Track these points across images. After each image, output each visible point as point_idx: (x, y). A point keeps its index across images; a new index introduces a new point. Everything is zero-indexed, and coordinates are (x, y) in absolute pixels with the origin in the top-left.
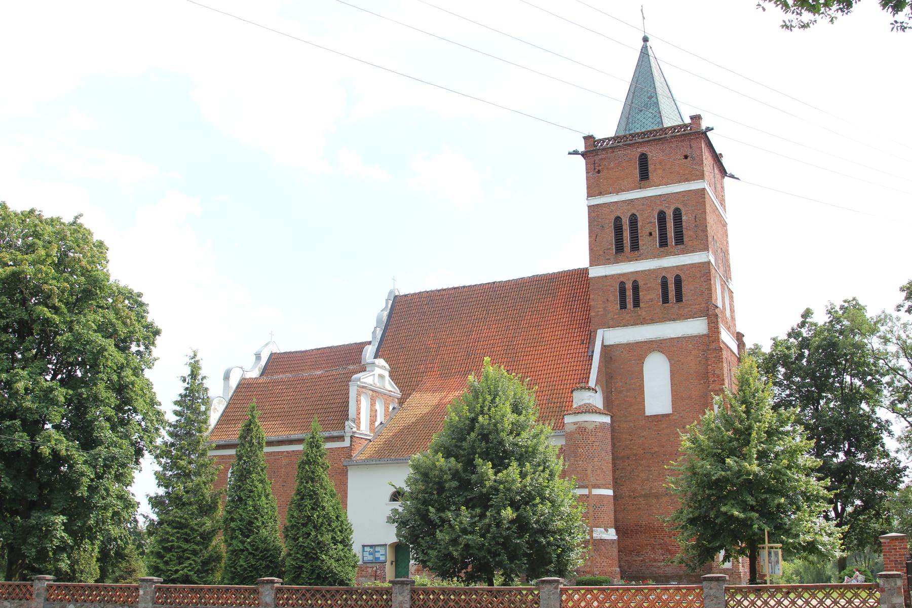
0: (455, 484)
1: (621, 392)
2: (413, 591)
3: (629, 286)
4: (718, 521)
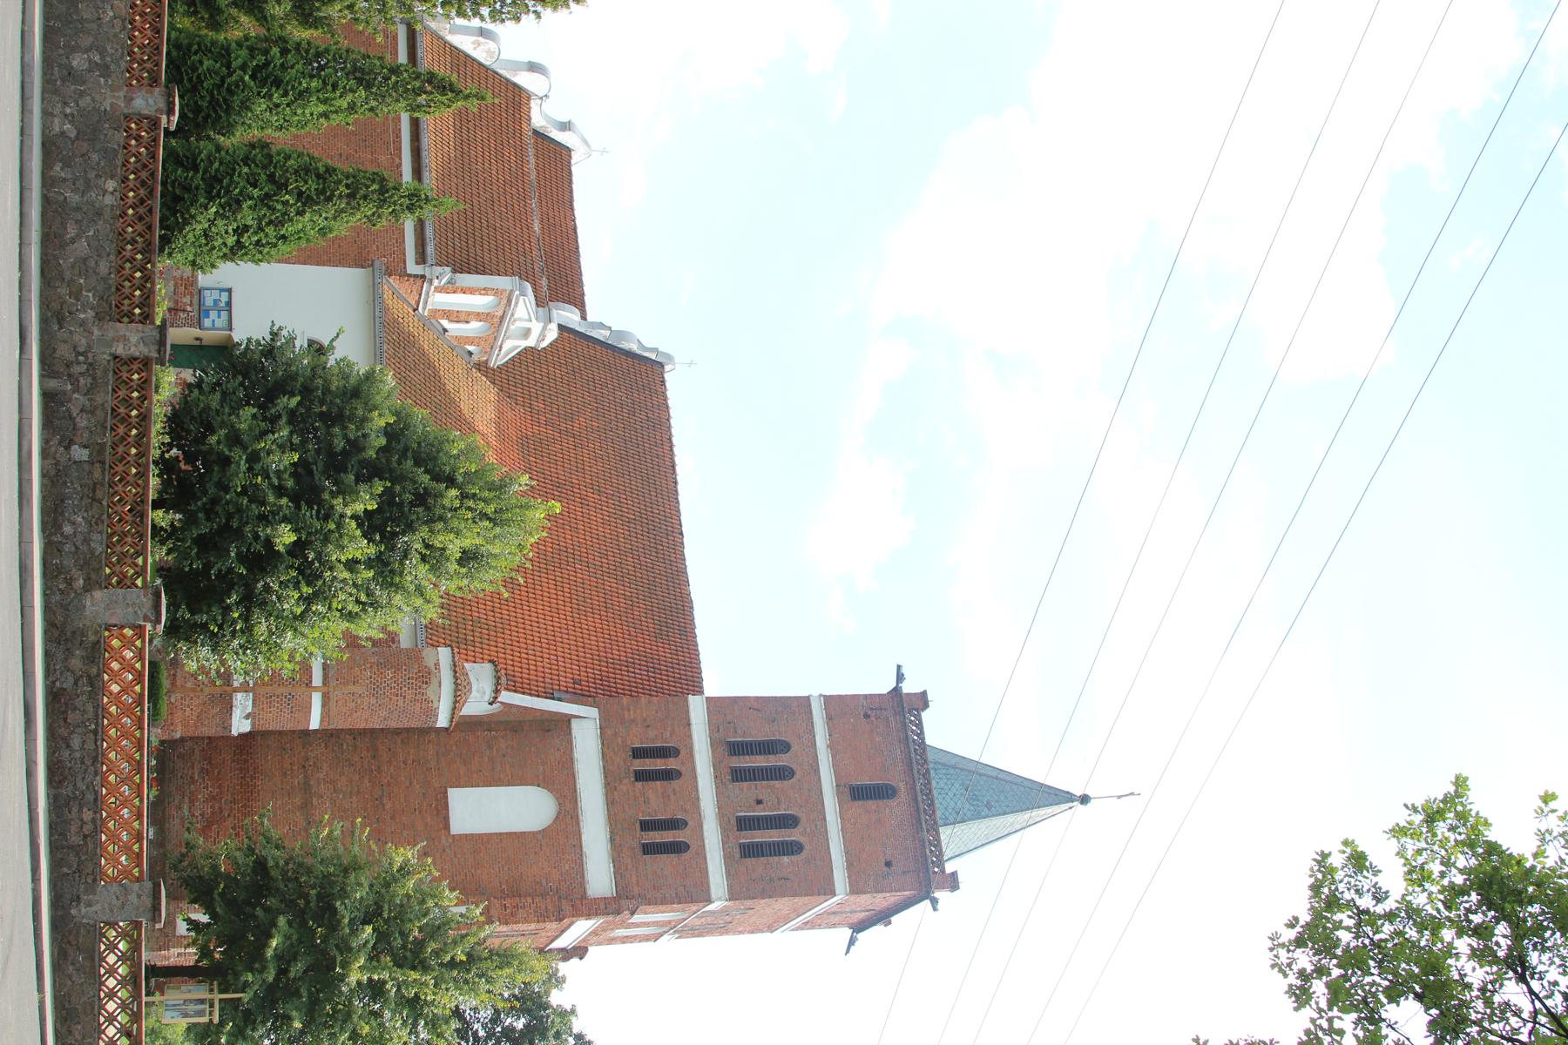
0: (339, 444)
1: (490, 747)
2: (146, 363)
3: (671, 764)
4: (259, 912)
